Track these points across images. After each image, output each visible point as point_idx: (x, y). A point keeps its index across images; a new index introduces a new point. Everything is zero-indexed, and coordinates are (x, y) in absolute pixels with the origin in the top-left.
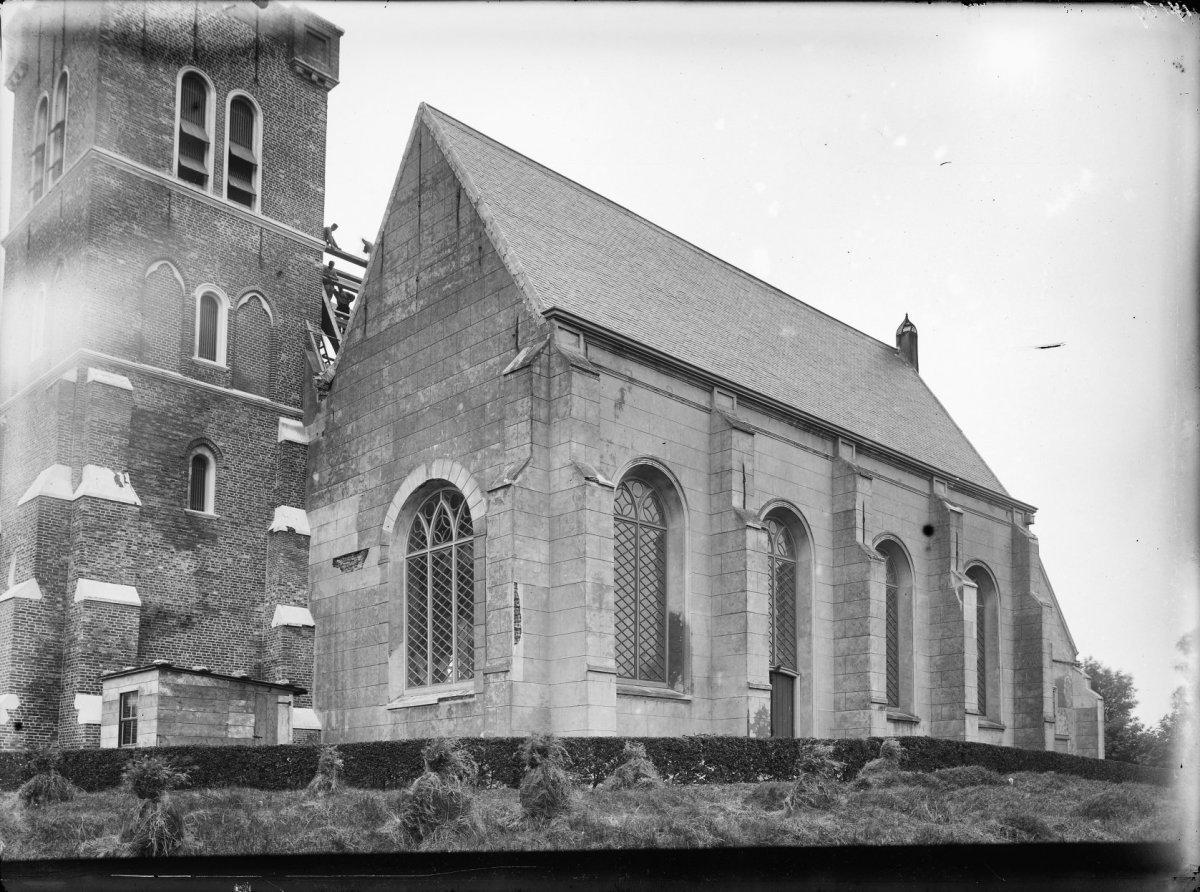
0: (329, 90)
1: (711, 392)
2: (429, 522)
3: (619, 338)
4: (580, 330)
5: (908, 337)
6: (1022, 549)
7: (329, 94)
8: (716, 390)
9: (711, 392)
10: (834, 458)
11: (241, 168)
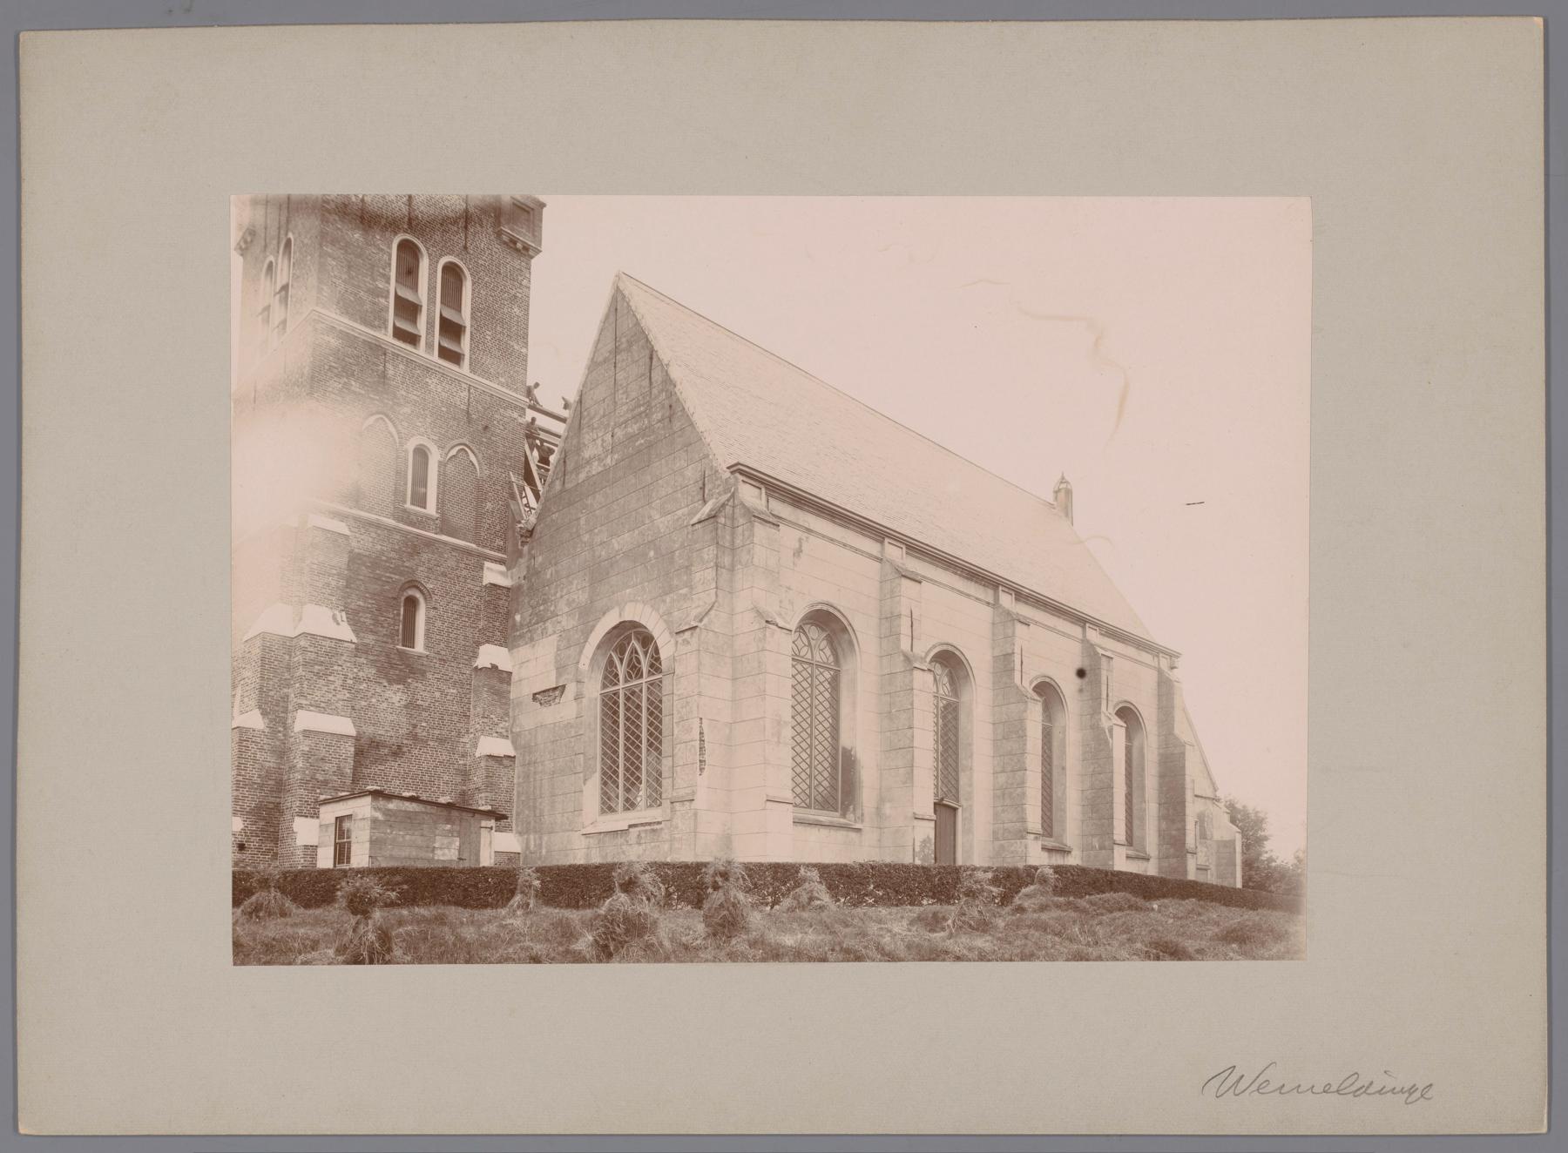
0: (532, 257)
1: (882, 542)
2: (621, 660)
3: (771, 480)
4: (763, 483)
5: (1064, 496)
6: (1165, 689)
7: (533, 261)
8: (887, 540)
9: (882, 542)
10: (995, 604)
11: (451, 329)
